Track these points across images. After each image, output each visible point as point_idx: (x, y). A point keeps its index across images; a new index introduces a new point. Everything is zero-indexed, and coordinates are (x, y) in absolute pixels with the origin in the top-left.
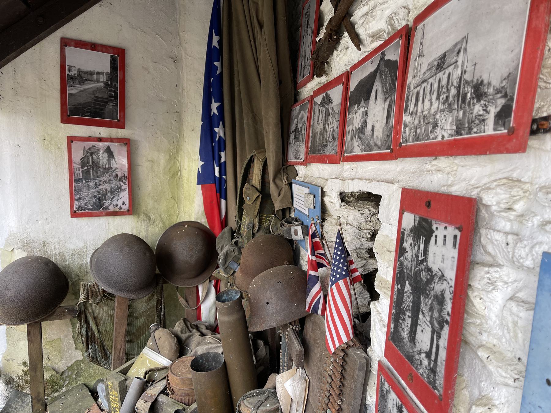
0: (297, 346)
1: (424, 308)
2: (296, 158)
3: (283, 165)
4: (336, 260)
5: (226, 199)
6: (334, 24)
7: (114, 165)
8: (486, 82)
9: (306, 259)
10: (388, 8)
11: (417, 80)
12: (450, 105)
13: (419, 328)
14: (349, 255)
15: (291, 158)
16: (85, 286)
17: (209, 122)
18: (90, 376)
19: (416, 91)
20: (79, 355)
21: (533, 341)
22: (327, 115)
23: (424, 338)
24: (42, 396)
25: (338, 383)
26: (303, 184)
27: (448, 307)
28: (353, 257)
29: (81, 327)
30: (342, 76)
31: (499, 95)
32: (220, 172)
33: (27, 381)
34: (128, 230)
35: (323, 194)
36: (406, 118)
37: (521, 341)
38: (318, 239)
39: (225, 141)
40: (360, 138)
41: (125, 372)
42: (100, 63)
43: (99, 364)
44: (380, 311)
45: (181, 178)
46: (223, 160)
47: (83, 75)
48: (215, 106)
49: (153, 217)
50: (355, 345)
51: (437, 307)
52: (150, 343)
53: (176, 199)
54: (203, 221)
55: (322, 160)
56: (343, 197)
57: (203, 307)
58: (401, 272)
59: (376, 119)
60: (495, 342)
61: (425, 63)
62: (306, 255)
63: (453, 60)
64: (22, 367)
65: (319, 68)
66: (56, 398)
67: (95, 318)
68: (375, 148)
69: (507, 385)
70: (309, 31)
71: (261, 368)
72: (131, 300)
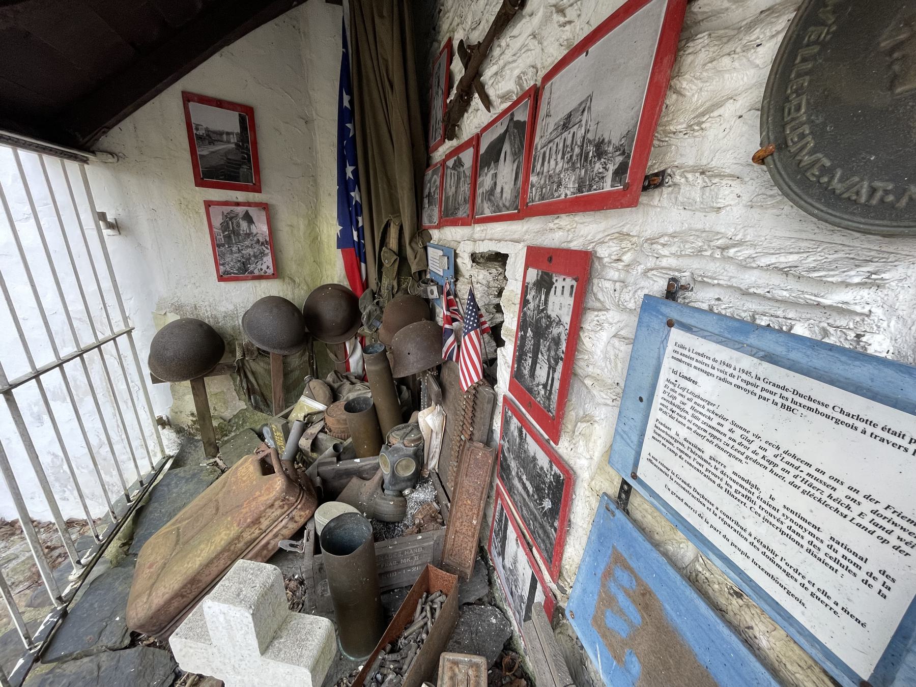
0: (435, 388)
1: (543, 349)
2: (430, 222)
3: (418, 229)
4: (467, 314)
5: (365, 263)
6: (464, 84)
7: (254, 229)
8: (606, 140)
9: (441, 315)
10: (518, 67)
11: (544, 140)
12: (573, 164)
13: (538, 366)
14: (479, 310)
15: (426, 222)
16: (241, 345)
17: (345, 187)
18: (255, 422)
19: (542, 151)
20: (242, 405)
21: (631, 368)
22: (459, 178)
23: (542, 373)
24: (213, 440)
25: (470, 415)
26: (436, 247)
27: (563, 346)
28: (483, 311)
29: (241, 381)
30: (471, 139)
31: (618, 153)
32: (358, 236)
33: (197, 429)
34: (274, 293)
35: (456, 256)
36: (533, 179)
37: (620, 370)
38: (452, 297)
39: (361, 206)
40: (490, 200)
41: (286, 416)
42: (229, 122)
43: (262, 411)
44: (506, 356)
45: (321, 242)
46: (360, 224)
47: (211, 135)
48: (349, 170)
49: (297, 280)
50: (484, 384)
51: (553, 347)
52: (306, 392)
53: (318, 263)
54: (346, 283)
55: (455, 223)
56: (474, 258)
57: (350, 360)
58: (524, 321)
59: (505, 180)
60: (599, 372)
61: (552, 123)
62: (441, 312)
63: (578, 120)
64: (191, 418)
65: (450, 132)
66: (226, 442)
67: (253, 373)
68: (504, 209)
69: (606, 405)
70: (440, 92)
71: (405, 408)
72: (285, 356)
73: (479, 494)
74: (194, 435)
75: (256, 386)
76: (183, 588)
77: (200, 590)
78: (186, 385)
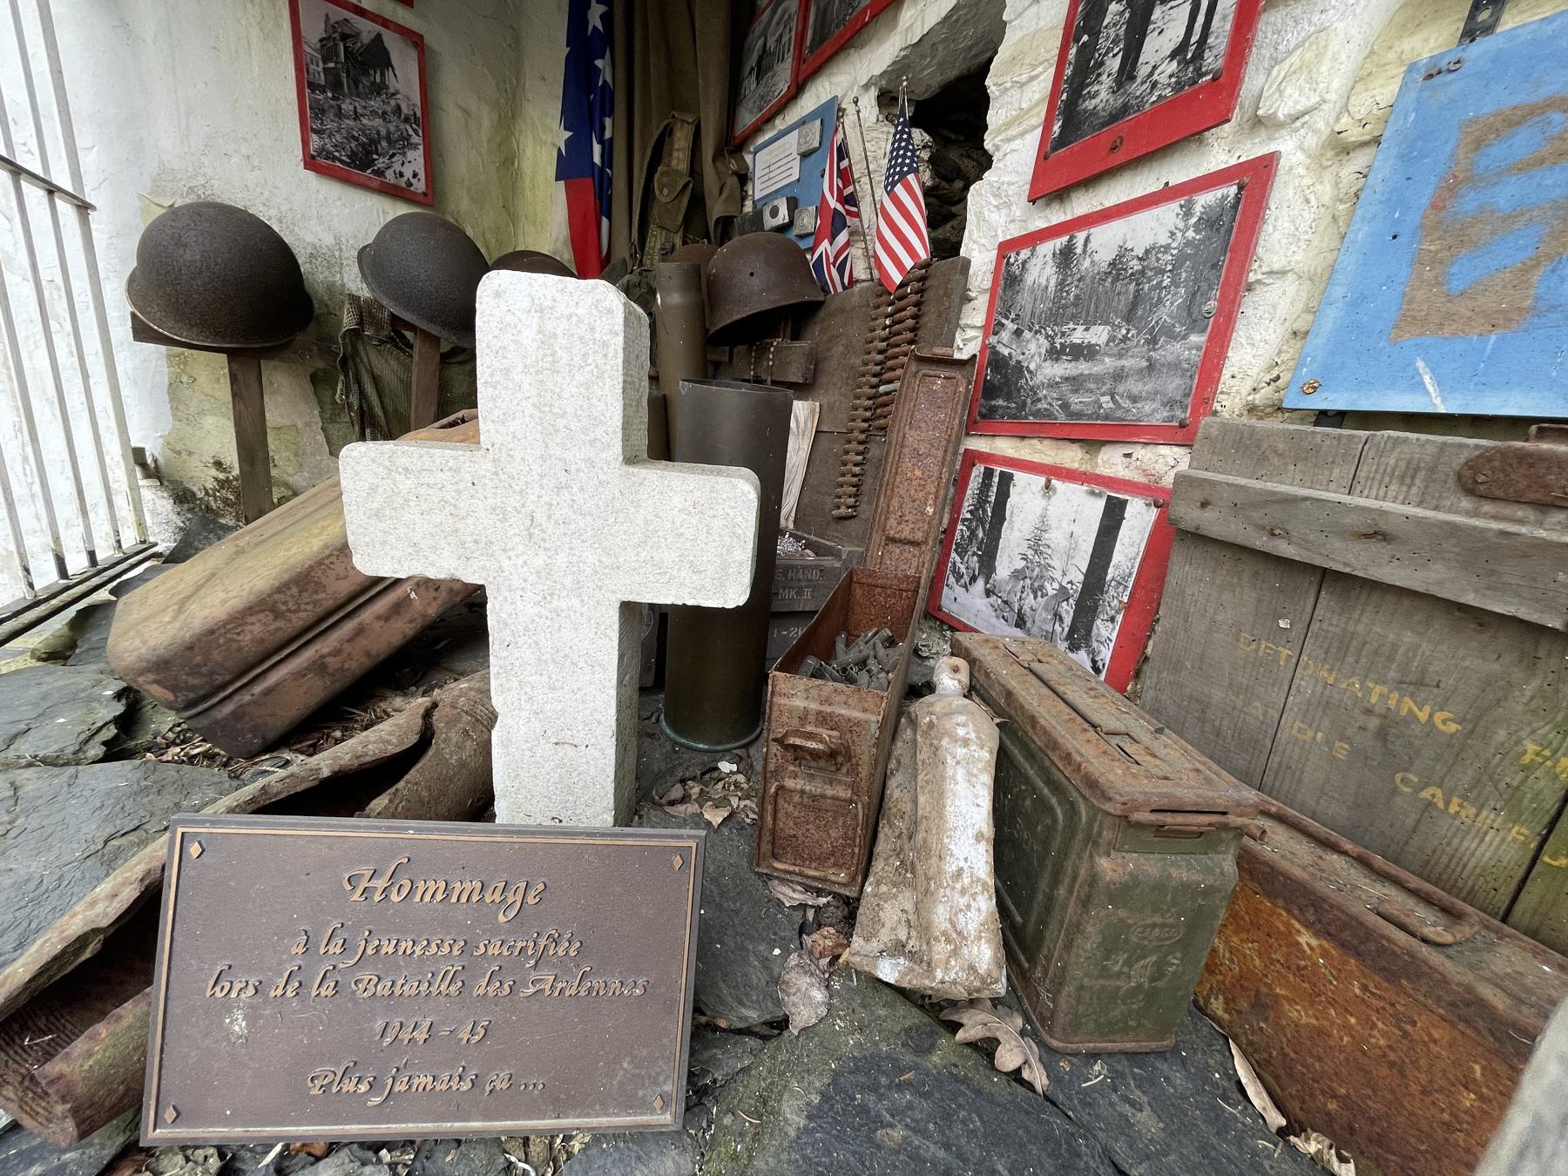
33: (226, 501)
39: (612, 93)
45: (519, 172)
46: (608, 135)
64: (214, 472)
67: (376, 380)
73: (940, 453)
74: (217, 514)
75: (378, 410)
76: (279, 590)
77: (320, 610)
78: (211, 372)
